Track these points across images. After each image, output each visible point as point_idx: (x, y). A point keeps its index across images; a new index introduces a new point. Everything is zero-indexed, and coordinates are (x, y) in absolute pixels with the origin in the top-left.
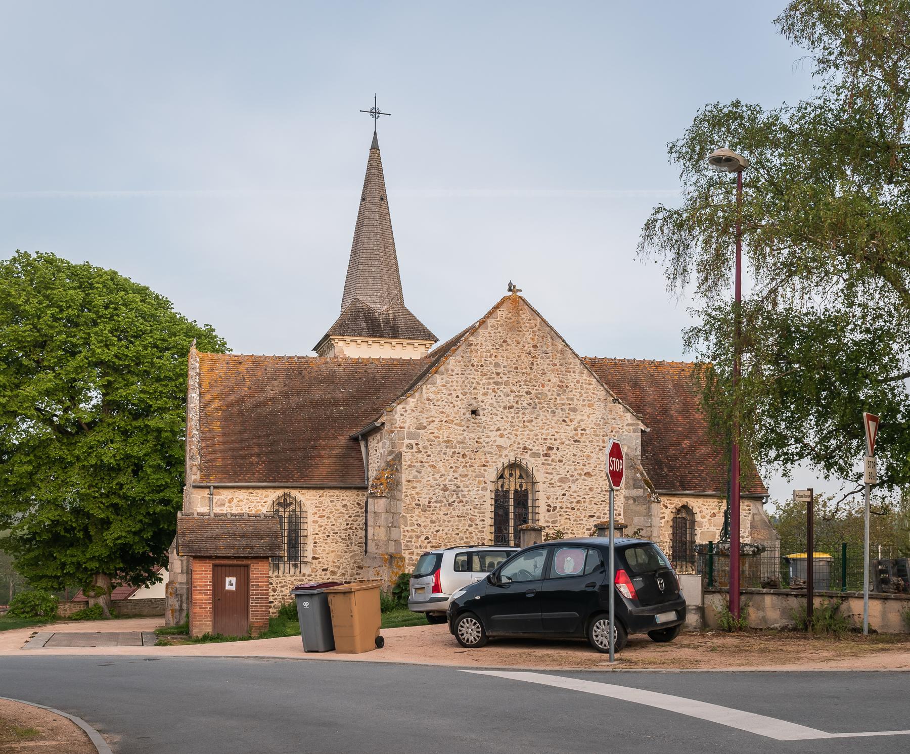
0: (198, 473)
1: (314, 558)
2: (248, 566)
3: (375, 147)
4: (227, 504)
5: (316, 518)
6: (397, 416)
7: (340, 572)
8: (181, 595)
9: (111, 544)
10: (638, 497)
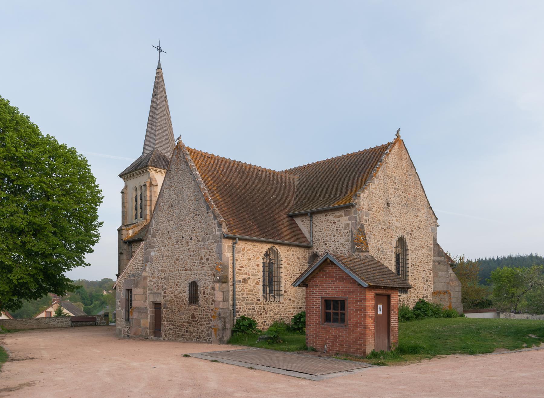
0: (226, 228)
1: (285, 292)
2: (389, 297)
3: (159, 68)
4: (242, 252)
5: (286, 265)
6: (361, 200)
7: (297, 300)
8: (224, 318)
9: (16, 283)
10: (441, 261)
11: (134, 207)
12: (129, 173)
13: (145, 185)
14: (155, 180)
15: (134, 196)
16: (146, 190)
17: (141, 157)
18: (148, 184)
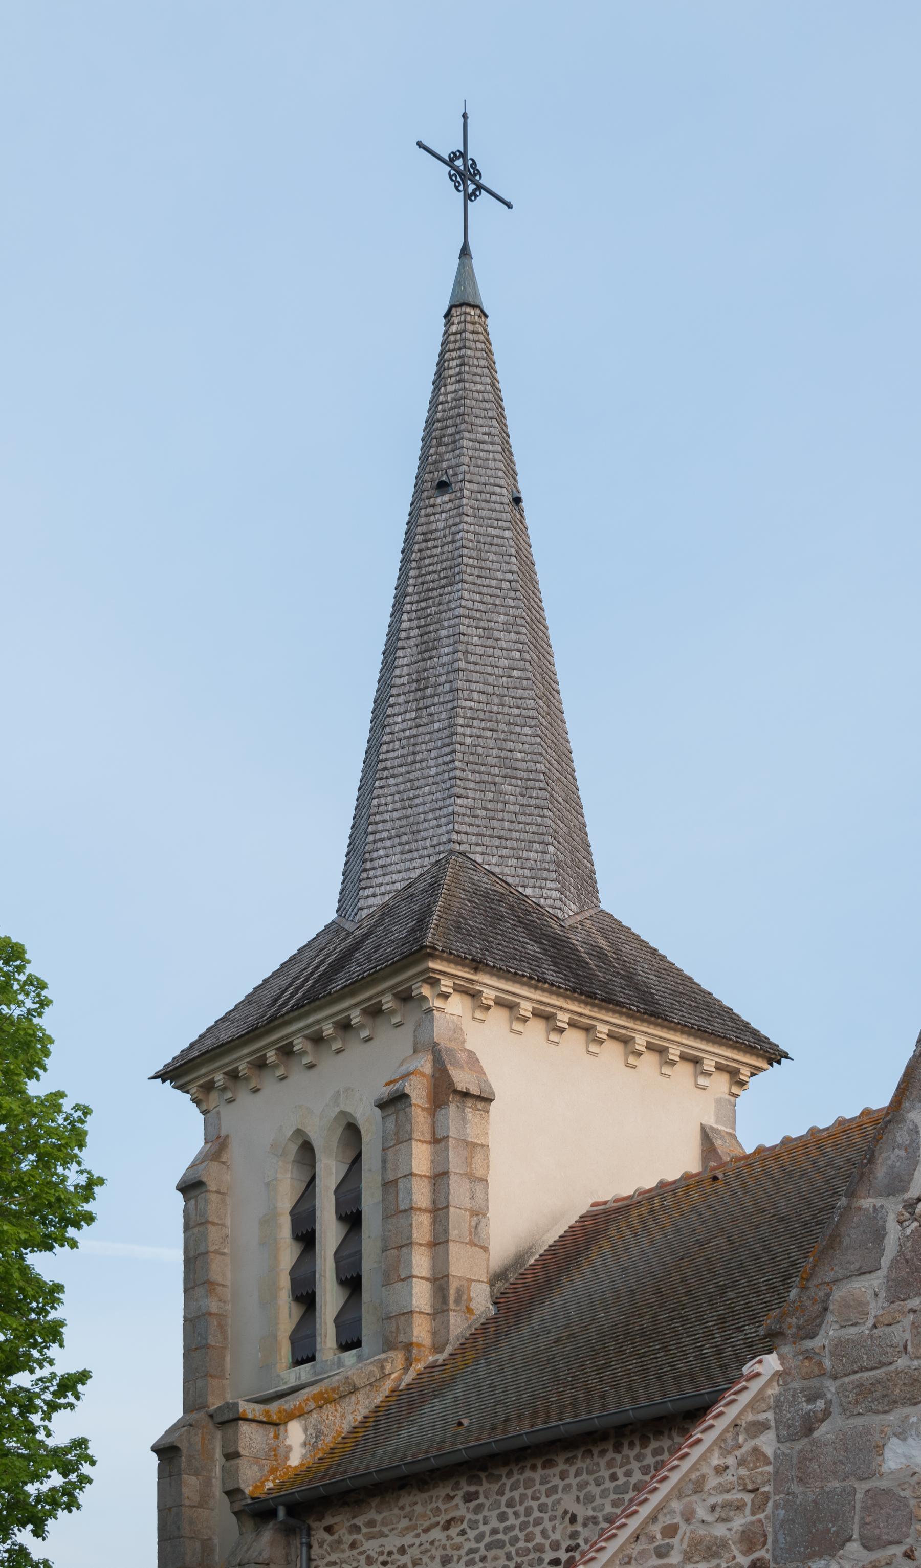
3: (464, 306)
11: (285, 1282)
12: (253, 1033)
13: (394, 1102)
14: (473, 1060)
15: (286, 1203)
16: (400, 1138)
17: (332, 929)
18: (418, 1092)
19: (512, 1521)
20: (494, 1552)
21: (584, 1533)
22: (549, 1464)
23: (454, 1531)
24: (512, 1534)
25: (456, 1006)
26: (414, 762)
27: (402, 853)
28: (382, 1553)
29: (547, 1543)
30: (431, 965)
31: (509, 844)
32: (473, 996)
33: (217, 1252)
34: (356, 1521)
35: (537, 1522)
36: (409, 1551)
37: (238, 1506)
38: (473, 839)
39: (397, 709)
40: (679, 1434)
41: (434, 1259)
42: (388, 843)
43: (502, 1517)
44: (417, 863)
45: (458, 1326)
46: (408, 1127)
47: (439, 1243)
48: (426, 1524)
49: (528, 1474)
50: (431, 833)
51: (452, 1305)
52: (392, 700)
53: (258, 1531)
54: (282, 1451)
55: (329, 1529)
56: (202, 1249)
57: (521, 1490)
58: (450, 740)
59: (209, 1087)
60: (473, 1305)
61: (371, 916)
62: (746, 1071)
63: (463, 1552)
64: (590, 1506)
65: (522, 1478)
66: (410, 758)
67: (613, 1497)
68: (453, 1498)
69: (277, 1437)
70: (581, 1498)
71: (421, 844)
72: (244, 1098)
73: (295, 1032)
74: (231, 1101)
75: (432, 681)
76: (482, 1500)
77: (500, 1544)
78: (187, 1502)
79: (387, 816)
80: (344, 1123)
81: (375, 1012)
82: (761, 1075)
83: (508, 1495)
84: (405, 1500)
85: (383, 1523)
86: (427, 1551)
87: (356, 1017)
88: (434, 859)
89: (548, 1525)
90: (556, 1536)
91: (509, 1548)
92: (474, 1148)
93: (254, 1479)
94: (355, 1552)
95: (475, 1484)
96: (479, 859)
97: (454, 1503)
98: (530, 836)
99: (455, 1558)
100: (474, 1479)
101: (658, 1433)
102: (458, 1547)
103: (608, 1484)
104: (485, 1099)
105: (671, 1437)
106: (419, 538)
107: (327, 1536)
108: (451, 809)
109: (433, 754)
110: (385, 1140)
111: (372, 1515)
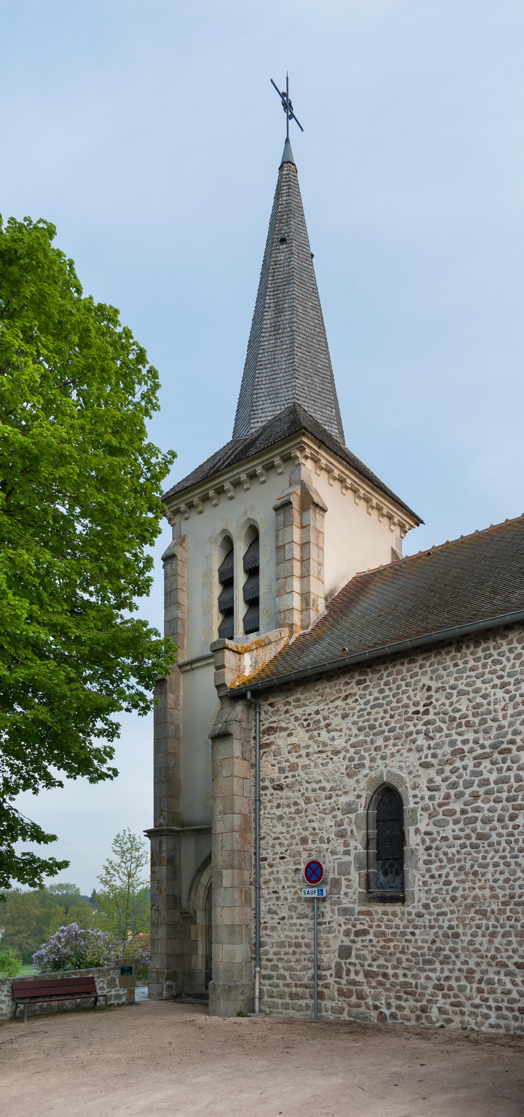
3: (287, 165)
11: (216, 603)
13: (284, 507)
19: (387, 692)
20: (376, 710)
21: (436, 696)
22: (412, 661)
23: (350, 701)
24: (388, 699)
25: (309, 464)
26: (275, 362)
27: (271, 403)
28: (304, 715)
29: (411, 703)
30: (305, 439)
31: (318, 405)
32: (315, 462)
33: (181, 589)
34: (288, 699)
35: (404, 692)
36: (321, 712)
37: (222, 694)
38: (304, 399)
39: (265, 339)
40: (501, 639)
41: (302, 584)
42: (264, 399)
43: (382, 691)
44: (278, 408)
45: (314, 617)
46: (291, 519)
47: (305, 576)
48: (332, 698)
49: (398, 667)
50: (284, 394)
51: (311, 607)
52: (263, 335)
53: (233, 707)
54: (242, 667)
55: (271, 705)
56: (174, 587)
57: (394, 676)
58: (291, 354)
59: (177, 512)
60: (319, 608)
61: (258, 431)
62: (407, 526)
63: (356, 711)
64: (440, 682)
65: (395, 670)
66: (273, 361)
67: (455, 675)
68: (350, 683)
69: (240, 660)
70: (434, 677)
71: (280, 399)
72: (194, 517)
73: (226, 481)
74: (187, 519)
75: (282, 326)
76: (368, 683)
77: (380, 706)
78: (169, 706)
79: (263, 386)
80: (248, 525)
81: (270, 467)
82: (413, 530)
83: (385, 679)
84: (319, 686)
85: (305, 699)
86: (333, 712)
87: (259, 470)
88: (286, 406)
89: (411, 693)
90: (418, 698)
91: (385, 707)
92: (319, 532)
93: (231, 680)
94: (287, 715)
95: (365, 675)
96: (306, 409)
97: (350, 686)
98: (325, 403)
99: (351, 715)
100: (363, 673)
101: (486, 639)
102: (353, 709)
103: (452, 669)
104: (324, 510)
105: (495, 640)
106: (272, 263)
107: (270, 709)
108: (294, 384)
109: (284, 359)
110: (277, 526)
111: (299, 695)
